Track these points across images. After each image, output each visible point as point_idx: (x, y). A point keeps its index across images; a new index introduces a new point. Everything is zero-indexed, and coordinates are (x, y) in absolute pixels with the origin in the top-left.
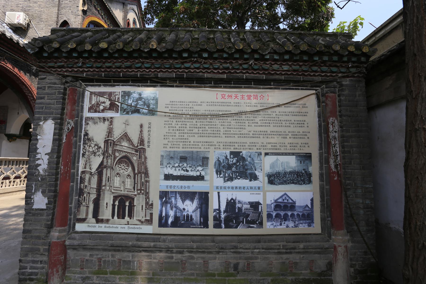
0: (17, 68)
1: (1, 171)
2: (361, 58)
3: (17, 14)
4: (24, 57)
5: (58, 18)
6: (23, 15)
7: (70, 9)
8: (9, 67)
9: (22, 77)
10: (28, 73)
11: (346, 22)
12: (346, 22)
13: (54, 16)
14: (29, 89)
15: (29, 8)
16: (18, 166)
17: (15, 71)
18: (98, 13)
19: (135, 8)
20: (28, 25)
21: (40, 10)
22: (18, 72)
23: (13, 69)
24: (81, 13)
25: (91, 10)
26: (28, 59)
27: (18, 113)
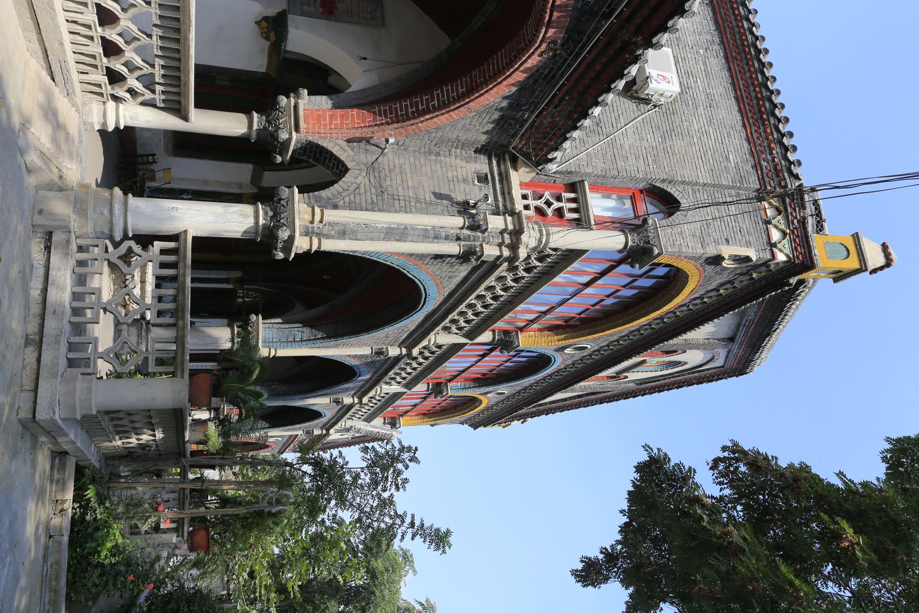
0: (527, 78)
1: (133, 5)
3: (673, 75)
4: (561, 100)
5: (683, 182)
6: (673, 92)
8: (530, 61)
9: (495, 90)
10: (509, 103)
13: (686, 173)
14: (454, 104)
15: (690, 103)
16: (160, 53)
17: (517, 72)
18: (710, 288)
19: (719, 362)
20: (646, 101)
21: (693, 132)
22: (511, 80)
23: (522, 69)
24: (711, 251)
25: (721, 274)
26: (555, 107)
27: (365, 59)
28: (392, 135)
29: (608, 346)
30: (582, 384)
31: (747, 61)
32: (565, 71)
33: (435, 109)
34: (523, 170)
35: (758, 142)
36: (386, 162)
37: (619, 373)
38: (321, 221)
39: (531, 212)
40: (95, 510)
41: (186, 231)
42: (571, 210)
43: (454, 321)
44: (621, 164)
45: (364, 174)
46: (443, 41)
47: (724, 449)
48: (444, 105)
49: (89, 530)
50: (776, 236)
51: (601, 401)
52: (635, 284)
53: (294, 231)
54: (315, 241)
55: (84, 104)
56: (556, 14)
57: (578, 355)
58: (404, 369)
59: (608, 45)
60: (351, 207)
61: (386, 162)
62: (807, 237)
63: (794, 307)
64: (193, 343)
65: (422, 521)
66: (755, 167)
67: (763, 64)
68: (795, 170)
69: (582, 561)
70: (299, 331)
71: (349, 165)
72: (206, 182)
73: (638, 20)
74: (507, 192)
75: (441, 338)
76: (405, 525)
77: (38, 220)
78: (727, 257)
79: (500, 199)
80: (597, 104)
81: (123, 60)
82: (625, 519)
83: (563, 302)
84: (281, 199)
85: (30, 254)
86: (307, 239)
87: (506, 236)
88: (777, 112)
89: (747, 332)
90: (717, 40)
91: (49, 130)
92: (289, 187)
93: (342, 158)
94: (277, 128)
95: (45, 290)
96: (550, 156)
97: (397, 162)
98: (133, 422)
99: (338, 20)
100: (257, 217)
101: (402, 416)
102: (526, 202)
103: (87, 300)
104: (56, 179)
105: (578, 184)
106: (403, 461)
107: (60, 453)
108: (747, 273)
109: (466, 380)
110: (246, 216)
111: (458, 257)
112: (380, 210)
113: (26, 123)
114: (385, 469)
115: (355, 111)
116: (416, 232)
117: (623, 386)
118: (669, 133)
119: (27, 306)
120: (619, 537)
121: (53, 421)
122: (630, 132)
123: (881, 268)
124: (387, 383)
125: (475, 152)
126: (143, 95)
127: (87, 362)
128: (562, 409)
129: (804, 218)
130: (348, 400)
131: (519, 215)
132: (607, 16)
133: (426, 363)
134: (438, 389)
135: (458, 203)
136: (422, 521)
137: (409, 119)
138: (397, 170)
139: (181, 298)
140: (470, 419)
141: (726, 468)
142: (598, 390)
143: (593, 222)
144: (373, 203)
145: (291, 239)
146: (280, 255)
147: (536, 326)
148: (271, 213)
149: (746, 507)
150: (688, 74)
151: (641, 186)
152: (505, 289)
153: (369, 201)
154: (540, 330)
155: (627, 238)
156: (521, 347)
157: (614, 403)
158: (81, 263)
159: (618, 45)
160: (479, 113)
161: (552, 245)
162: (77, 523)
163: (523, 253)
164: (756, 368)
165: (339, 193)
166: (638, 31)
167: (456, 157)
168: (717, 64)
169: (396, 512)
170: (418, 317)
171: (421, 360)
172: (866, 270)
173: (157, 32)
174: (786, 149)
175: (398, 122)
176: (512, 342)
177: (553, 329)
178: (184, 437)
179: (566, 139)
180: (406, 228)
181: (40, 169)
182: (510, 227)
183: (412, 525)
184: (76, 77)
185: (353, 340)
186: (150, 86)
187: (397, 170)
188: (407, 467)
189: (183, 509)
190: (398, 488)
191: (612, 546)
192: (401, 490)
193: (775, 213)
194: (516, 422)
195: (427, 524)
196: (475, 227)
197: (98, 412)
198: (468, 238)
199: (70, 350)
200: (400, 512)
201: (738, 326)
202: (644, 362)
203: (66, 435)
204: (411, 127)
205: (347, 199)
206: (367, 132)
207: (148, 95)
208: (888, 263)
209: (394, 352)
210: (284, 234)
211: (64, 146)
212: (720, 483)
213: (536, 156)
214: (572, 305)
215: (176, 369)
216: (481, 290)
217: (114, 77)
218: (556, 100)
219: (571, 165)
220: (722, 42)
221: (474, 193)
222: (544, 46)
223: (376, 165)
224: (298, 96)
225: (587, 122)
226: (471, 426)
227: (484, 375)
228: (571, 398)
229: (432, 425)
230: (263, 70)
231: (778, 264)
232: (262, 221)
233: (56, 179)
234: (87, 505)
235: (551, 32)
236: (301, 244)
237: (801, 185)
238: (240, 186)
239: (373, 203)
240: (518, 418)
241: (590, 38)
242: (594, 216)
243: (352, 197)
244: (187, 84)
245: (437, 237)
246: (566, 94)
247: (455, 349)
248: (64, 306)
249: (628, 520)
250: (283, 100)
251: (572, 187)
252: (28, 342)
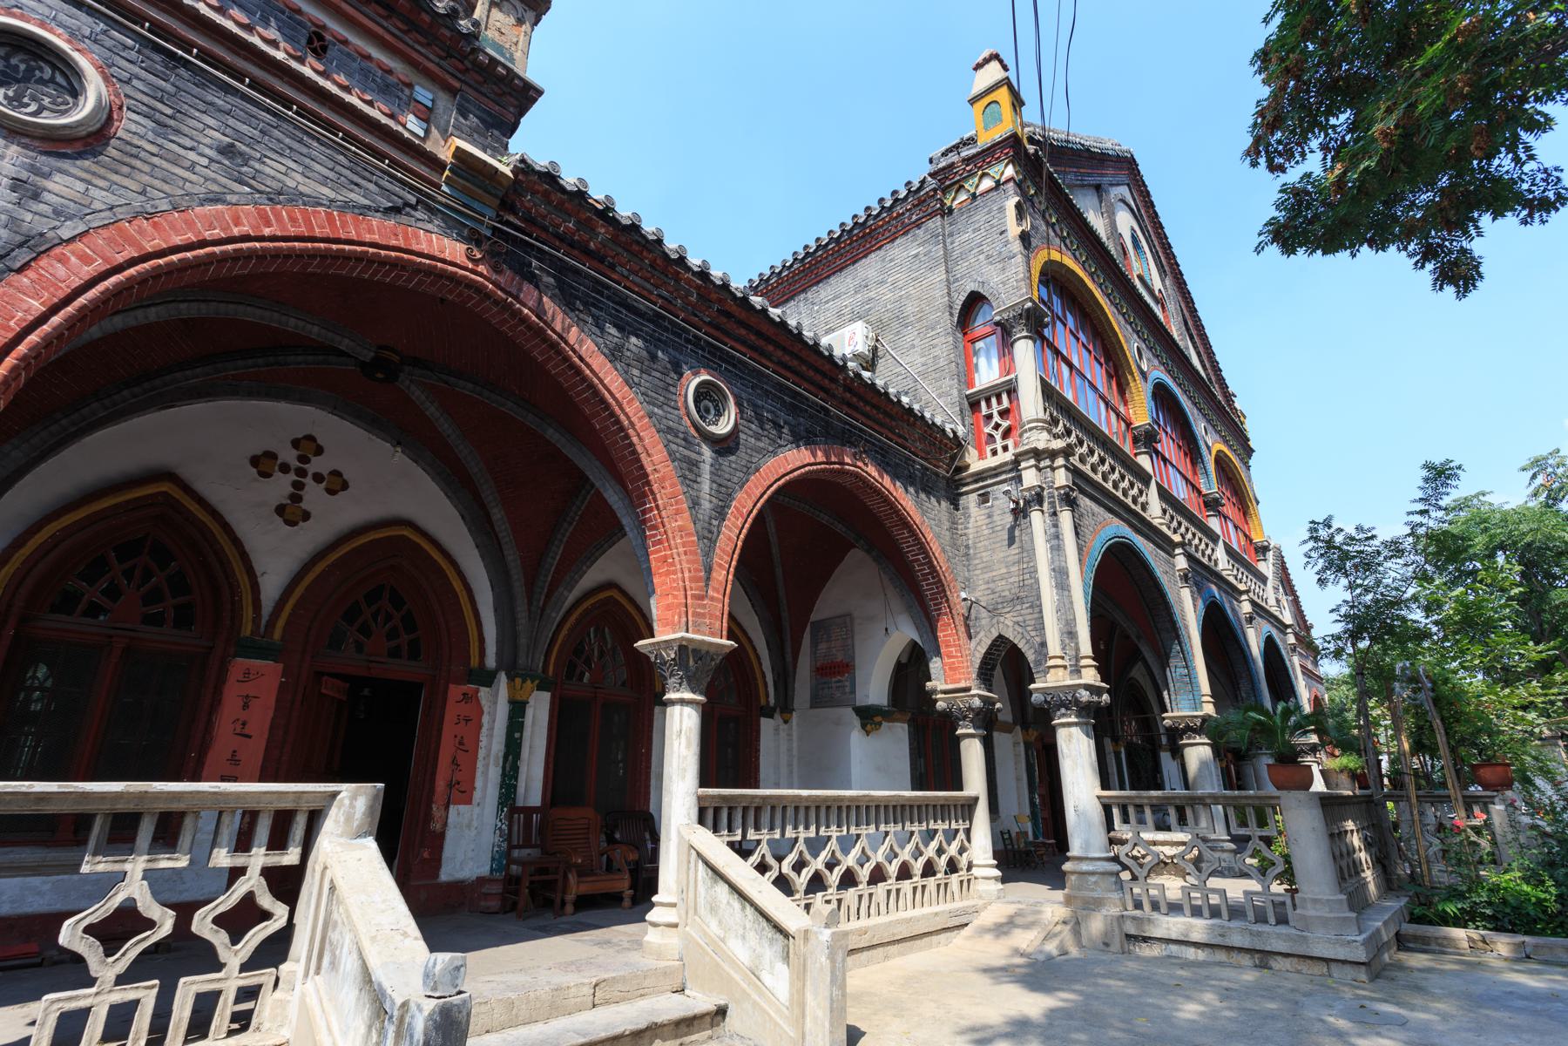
0: (887, 473)
2: (477, 691)
4: (900, 436)
5: (949, 294)
7: (981, 252)
13: (939, 294)
19: (1124, 191)
20: (875, 350)
22: (891, 488)
24: (1017, 246)
28: (959, 596)
29: (1131, 324)
30: (1175, 336)
31: (817, 262)
32: (876, 438)
33: (927, 556)
34: (968, 459)
35: (893, 230)
36: (985, 598)
37: (1157, 301)
38: (1063, 658)
39: (1010, 442)
40: (1475, 903)
41: (1099, 797)
42: (999, 402)
43: (1135, 501)
44: (942, 362)
45: (1002, 619)
46: (856, 556)
47: (1254, 164)
48: (923, 549)
49: (1508, 910)
50: (987, 184)
51: (1193, 312)
52: (1060, 314)
53: (1079, 686)
54: (1084, 662)
55: (980, 897)
56: (833, 459)
57: (1146, 354)
58: (1197, 547)
59: (849, 405)
60: (1040, 627)
61: (985, 598)
62: (983, 151)
63: (1056, 136)
64: (1212, 786)
65: (1415, 501)
66: (919, 227)
67: (818, 247)
68: (916, 185)
69: (1441, 288)
70: (1176, 670)
71: (995, 634)
72: (1018, 779)
74: (994, 472)
75: (1155, 511)
76: (1425, 521)
77: (1116, 946)
78: (1020, 229)
79: (1003, 477)
80: (899, 401)
82: (1365, 248)
83: (1093, 386)
84: (1046, 701)
85: (1156, 958)
86: (1083, 670)
87: (1042, 464)
88: (861, 221)
89: (1089, 175)
90: (802, 296)
91: (1017, 932)
92: (1031, 694)
93: (989, 642)
94: (970, 709)
95: (1196, 945)
96: (951, 435)
97: (983, 587)
98: (1341, 855)
99: (853, 659)
100: (1069, 725)
101: (1251, 541)
102: (1000, 450)
103: (1199, 903)
104: (1068, 927)
106: (1332, 536)
107: (1398, 940)
108: (1031, 201)
109: (1195, 473)
110: (1070, 736)
111: (1073, 511)
112: (1039, 597)
113: (1017, 952)
114: (1346, 556)
115: (940, 634)
116: (1056, 558)
117: (1170, 291)
118: (901, 320)
119: (1220, 964)
120: (1392, 249)
121: (1366, 943)
122: (908, 359)
123: (1001, 62)
124: (1216, 564)
125: (957, 510)
126: (801, 853)
127: (1279, 906)
128: (1211, 354)
129: (964, 160)
130: (1246, 608)
131: (1017, 456)
132: (827, 411)
133: (1185, 523)
134: (1212, 505)
135: (1016, 519)
136: (1415, 501)
137: (940, 581)
138: (991, 585)
139: (1178, 802)
140: (1242, 460)
141: (1280, 155)
142: (1180, 318)
143: (1008, 378)
144: (1031, 607)
145: (1087, 687)
146: (1105, 697)
147: (1122, 409)
148: (1063, 710)
149: (1330, 112)
150: (840, 315)
151: (960, 336)
152: (1092, 452)
153: (1030, 610)
154: (1126, 404)
155: (1019, 339)
156: (1149, 421)
157: (1193, 295)
158: (1155, 906)
159: (848, 395)
160: (924, 513)
161: (1041, 415)
162: (1499, 924)
163: (1058, 444)
164: (1124, 148)
165: (1028, 642)
166: (834, 380)
167: (966, 528)
168: (824, 291)
169: (1409, 535)
170: (1140, 542)
171: (1183, 530)
172: (1007, 78)
173: (882, 828)
174: (896, 200)
175: (944, 591)
176: (1146, 432)
177: (1122, 389)
178: (1349, 796)
179: (933, 423)
180: (1054, 570)
181: (1061, 941)
182: (1032, 462)
183: (1423, 513)
184: (958, 904)
185: (1176, 610)
186: (931, 835)
187: (991, 585)
188: (1340, 530)
189: (1449, 797)
190: (1373, 537)
191: (1410, 256)
192: (1374, 532)
193: (963, 191)
194: (1236, 405)
195: (1420, 494)
196: (1039, 499)
197: (1341, 892)
198: (1052, 504)
199: (1265, 921)
200: (1408, 530)
201: (1083, 186)
202: (1140, 278)
203: (1378, 931)
204: (947, 577)
205: (1033, 634)
206: (959, 620)
207: (961, 835)
208: (995, 57)
209: (1181, 563)
210: (1084, 696)
211: (1030, 919)
212: (1303, 155)
213: (952, 449)
214: (1093, 375)
215: (1268, 805)
216: (1098, 478)
217: (952, 867)
218: (900, 441)
219: (953, 412)
220: (804, 291)
221: (1001, 504)
222: (859, 464)
223: (990, 608)
224: (934, 691)
225: (916, 407)
226: (1250, 457)
227: (1186, 454)
228: (1195, 347)
229: (1258, 503)
230: (906, 726)
231: (1017, 172)
232: (1073, 719)
233: (1068, 927)
234: (1468, 913)
235: (847, 460)
236: (1090, 676)
237: (930, 175)
238: (1016, 744)
239: (1031, 607)
240: (1230, 401)
242: (1001, 376)
243: (1029, 628)
244: (946, 798)
245: (1057, 536)
246: (894, 433)
247: (1165, 495)
248: (1213, 925)
249: (1366, 245)
250: (941, 705)
251: (974, 405)
252: (1263, 966)
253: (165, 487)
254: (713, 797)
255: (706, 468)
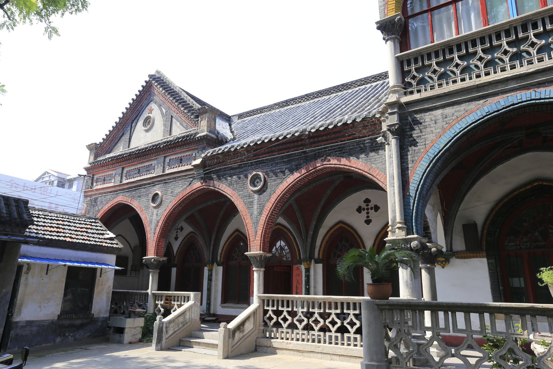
4: (349, 136)
11: (47, 274)
12: (47, 274)
22: (347, 163)
23: (339, 163)
26: (355, 134)
59: (314, 143)
73: (300, 143)
81: (177, 308)
105: (468, 42)
159: (312, 140)
241: (316, 150)
253: (341, 225)
254: (281, 297)
255: (256, 202)
